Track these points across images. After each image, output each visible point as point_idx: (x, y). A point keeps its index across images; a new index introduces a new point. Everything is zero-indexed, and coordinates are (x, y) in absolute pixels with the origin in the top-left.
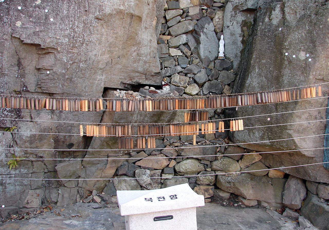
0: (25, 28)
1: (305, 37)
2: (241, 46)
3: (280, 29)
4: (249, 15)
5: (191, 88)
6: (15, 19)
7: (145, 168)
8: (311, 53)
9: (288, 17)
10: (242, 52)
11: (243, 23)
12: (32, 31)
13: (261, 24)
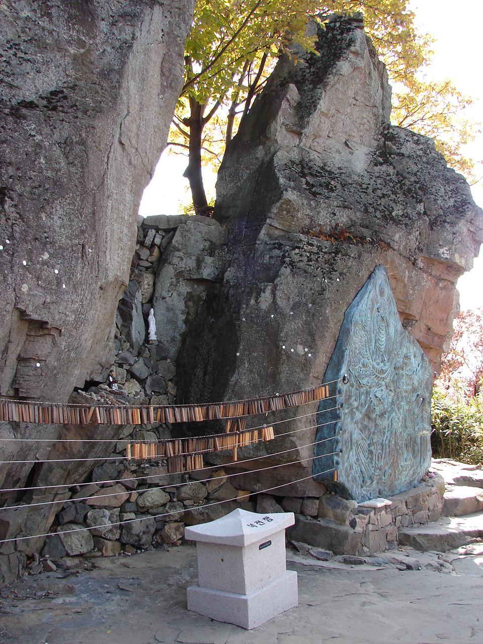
0: (33, 295)
1: (301, 328)
2: (182, 327)
3: (272, 316)
4: (196, 286)
5: (131, 385)
6: (21, 280)
7: (100, 507)
8: (310, 347)
9: (279, 301)
10: (184, 336)
11: (188, 296)
12: (41, 301)
13: (244, 306)
